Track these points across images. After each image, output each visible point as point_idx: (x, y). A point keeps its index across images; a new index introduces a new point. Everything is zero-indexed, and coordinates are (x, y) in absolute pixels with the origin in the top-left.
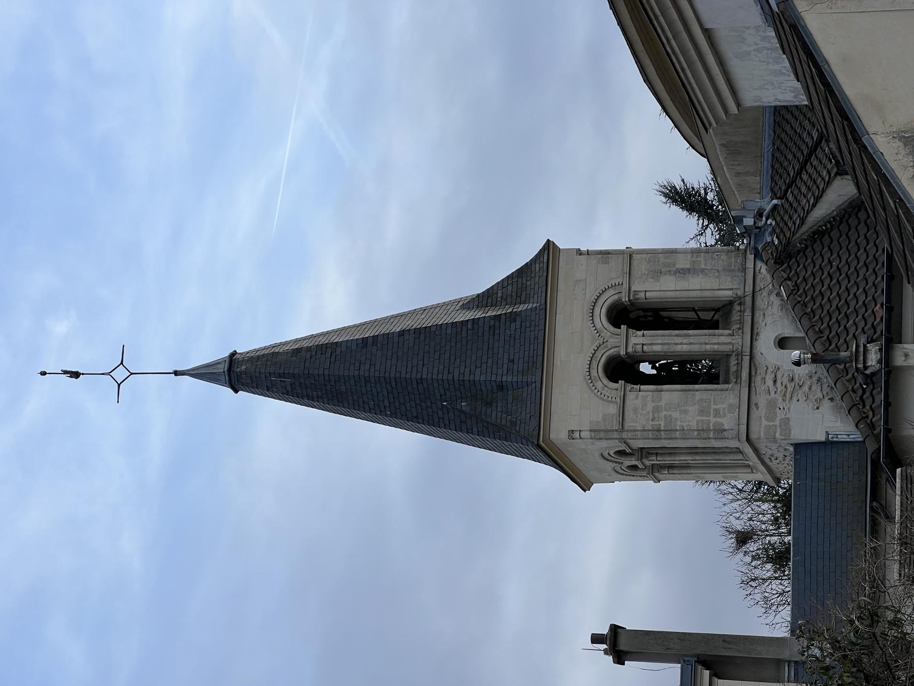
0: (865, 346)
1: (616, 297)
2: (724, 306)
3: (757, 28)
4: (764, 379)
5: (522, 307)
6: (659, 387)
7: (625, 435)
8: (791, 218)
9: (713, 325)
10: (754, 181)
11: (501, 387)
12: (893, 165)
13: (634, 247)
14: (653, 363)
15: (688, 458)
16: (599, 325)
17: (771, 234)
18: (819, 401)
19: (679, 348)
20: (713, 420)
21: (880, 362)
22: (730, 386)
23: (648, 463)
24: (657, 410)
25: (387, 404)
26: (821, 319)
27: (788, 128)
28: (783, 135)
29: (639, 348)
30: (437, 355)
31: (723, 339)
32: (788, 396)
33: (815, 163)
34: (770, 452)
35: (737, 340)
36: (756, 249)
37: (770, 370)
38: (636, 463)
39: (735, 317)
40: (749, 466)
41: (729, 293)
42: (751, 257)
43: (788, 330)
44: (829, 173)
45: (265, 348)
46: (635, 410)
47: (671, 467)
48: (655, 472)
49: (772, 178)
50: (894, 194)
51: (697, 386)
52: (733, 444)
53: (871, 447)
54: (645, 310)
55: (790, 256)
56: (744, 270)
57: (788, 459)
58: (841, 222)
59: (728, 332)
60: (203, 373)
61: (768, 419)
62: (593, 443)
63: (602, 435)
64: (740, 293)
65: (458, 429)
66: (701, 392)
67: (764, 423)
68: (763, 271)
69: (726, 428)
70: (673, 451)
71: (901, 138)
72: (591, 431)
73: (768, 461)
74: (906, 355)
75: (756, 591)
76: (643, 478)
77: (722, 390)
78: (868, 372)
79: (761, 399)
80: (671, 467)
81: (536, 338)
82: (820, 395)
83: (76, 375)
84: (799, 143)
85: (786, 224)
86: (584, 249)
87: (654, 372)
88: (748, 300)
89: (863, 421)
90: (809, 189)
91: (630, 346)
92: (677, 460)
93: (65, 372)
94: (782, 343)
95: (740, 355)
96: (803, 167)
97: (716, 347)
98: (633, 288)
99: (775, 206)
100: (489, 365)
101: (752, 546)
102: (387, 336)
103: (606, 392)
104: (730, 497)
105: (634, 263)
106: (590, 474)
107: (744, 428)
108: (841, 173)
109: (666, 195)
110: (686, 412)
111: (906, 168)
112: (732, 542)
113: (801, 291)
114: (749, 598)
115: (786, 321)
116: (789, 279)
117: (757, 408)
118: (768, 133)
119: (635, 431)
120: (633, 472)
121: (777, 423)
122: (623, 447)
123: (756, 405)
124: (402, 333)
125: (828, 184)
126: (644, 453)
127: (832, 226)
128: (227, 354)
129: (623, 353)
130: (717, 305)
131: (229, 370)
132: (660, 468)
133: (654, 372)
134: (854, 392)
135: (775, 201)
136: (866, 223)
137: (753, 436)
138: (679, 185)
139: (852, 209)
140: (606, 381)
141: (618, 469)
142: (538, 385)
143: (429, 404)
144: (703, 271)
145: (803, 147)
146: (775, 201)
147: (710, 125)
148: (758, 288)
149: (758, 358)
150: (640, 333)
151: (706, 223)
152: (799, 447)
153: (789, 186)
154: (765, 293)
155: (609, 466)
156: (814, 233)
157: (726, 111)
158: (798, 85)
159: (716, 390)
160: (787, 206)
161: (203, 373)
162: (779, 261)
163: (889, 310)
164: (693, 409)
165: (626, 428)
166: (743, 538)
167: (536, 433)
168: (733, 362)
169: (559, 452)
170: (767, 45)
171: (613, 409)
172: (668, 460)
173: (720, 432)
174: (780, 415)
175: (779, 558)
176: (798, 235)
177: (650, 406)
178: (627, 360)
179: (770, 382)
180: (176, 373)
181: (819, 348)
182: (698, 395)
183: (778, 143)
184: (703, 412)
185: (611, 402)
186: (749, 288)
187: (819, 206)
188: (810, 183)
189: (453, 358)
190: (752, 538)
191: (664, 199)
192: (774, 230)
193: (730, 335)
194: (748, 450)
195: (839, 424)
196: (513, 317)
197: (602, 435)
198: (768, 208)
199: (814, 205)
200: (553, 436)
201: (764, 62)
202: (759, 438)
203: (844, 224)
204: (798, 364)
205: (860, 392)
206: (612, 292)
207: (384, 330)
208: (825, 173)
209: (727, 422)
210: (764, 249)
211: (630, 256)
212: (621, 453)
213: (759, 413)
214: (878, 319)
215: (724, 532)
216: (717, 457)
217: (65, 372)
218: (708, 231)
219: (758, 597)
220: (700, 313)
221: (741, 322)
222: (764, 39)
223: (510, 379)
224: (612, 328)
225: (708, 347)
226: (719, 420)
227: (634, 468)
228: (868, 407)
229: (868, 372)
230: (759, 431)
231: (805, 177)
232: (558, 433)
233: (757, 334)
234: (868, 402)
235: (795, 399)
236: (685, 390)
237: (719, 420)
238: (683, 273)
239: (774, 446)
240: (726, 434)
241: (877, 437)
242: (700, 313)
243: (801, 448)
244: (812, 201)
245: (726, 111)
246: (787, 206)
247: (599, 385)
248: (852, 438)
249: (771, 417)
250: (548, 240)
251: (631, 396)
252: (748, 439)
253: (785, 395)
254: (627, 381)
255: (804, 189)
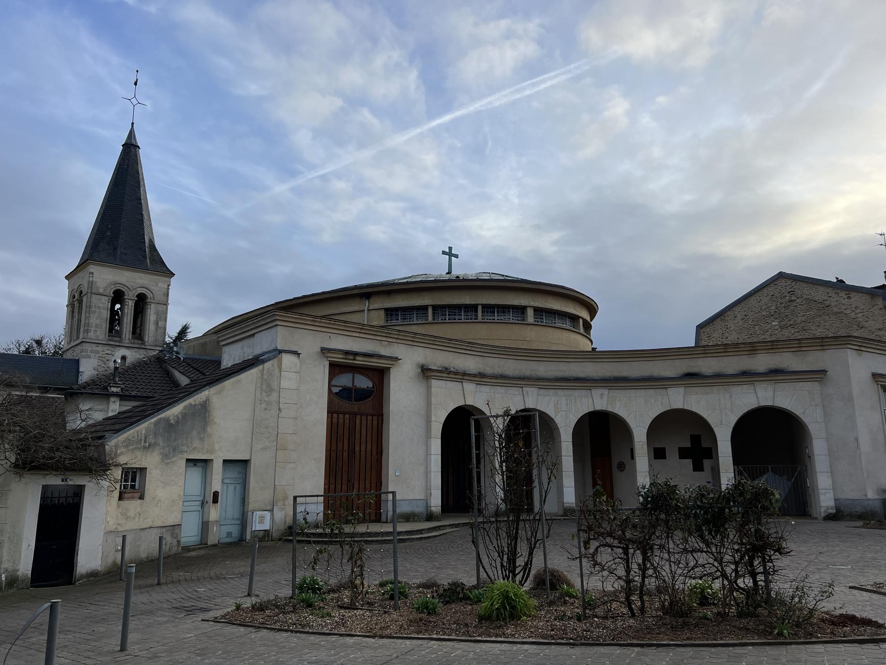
0: (120, 387)
1: (149, 297)
2: (142, 338)
3: (253, 353)
4: (109, 350)
5: (148, 261)
6: (109, 310)
7: (89, 294)
8: (175, 364)
9: (134, 333)
10: (191, 352)
11: (115, 249)
12: (196, 397)
13: (169, 306)
14: (120, 309)
15: (76, 319)
16: (138, 289)
17: (169, 356)
18: (97, 370)
19: (125, 319)
20: (93, 329)
21: (113, 392)
22: (107, 337)
23: (75, 303)
24: (99, 308)
25: (112, 204)
26: (133, 372)
27: (210, 365)
28: (208, 363)
29: (127, 304)
30: (131, 226)
31: (127, 336)
32: (100, 358)
33: (196, 373)
34: (76, 350)
35: (127, 341)
36: (164, 351)
37: (113, 353)
38: (76, 298)
39: (136, 341)
40: (71, 342)
41: (147, 340)
42: (161, 349)
43: (128, 361)
44: (192, 377)
45: (140, 161)
46: (99, 299)
47: (73, 312)
48: (71, 305)
49: (191, 358)
50: (185, 396)
51: (108, 324)
52: (81, 336)
53: (75, 387)
54: (143, 308)
55: (159, 362)
56: (156, 346)
57: (73, 357)
58: (171, 381)
59: (130, 338)
60: (131, 134)
61: (91, 350)
62: (86, 281)
63: (90, 285)
64: (146, 344)
65: (98, 230)
66: (105, 326)
67: (90, 349)
68: (155, 353)
69: (89, 334)
70: (80, 313)
71: (206, 400)
72: (92, 281)
73: (72, 349)
74: (114, 402)
75: (14, 346)
76: (69, 301)
77: (105, 334)
78: (108, 387)
79: (100, 348)
80: (73, 312)
81: (135, 265)
82: (100, 370)
83: (136, 84)
84: (204, 368)
85: (173, 362)
86: (170, 287)
87: (116, 309)
88: (143, 347)
89: (87, 384)
90: (186, 370)
91: (128, 300)
92: (76, 315)
93: (137, 80)
94: (124, 358)
95: (120, 342)
96: (195, 369)
97: (125, 333)
98: (152, 304)
99: (180, 359)
100: (125, 246)
101: (35, 345)
102: (141, 209)
103: (109, 289)
104: (58, 339)
105: (162, 306)
106: (72, 280)
107: (88, 341)
108: (192, 381)
109: (186, 325)
110: (97, 319)
111: (195, 401)
112: (37, 338)
113: (145, 366)
114: (11, 343)
115: (133, 360)
116: (151, 361)
117: (96, 347)
118: (209, 358)
119: (91, 299)
120: (72, 297)
121: (89, 354)
122: (84, 293)
123: (98, 346)
124: (142, 214)
125: (188, 377)
126: (80, 302)
127: (171, 378)
128: (139, 145)
129: (126, 297)
130: (142, 335)
131: (132, 144)
132: (73, 308)
133: (116, 309)
134: (100, 382)
135: (182, 359)
136: (171, 390)
137: (84, 344)
138: (188, 331)
139: (176, 384)
140: (114, 289)
141: (74, 291)
142: (115, 263)
143: (110, 220)
144: (157, 330)
145: (203, 369)
146: (182, 359)
147: (217, 335)
148: (147, 350)
149: (118, 348)
150: (133, 305)
151: (173, 339)
152: (78, 361)
153: (188, 364)
154: (145, 353)
155: (76, 287)
156: (168, 371)
157: (221, 341)
158: (229, 366)
159: (106, 331)
160: (180, 362)
161: (131, 134)
162: (158, 358)
163: (134, 397)
164: (98, 322)
165: (92, 295)
166: (39, 343)
167: (93, 259)
168: (117, 339)
169: (85, 267)
170: (246, 356)
171: (101, 291)
172: (76, 311)
173: (88, 331)
174: (92, 355)
175: (27, 351)
176: (168, 366)
177: (101, 305)
178: (122, 299)
179: (107, 352)
180: (133, 123)
181: (120, 370)
182: (104, 324)
183: (205, 361)
184: (97, 326)
185: (104, 290)
186: (148, 347)
187: (180, 373)
188: (189, 371)
189: (130, 232)
190: (38, 346)
191: (184, 325)
192: (171, 358)
193: (129, 338)
194: (78, 342)
195: (86, 377)
196: (145, 257)
197: (90, 285)
198: (180, 356)
199: (180, 372)
200: (91, 266)
201: (4, 631)
202: (83, 346)
203: (171, 382)
204: (115, 361)
205: (100, 384)
206: (151, 296)
207: (144, 208)
208: (192, 376)
209: (91, 335)
210: (163, 353)
211: (165, 304)
212: (81, 292)
213: (94, 347)
214: (131, 392)
215: (42, 335)
216: (76, 330)
217: (137, 80)
218: (170, 339)
219: (11, 346)
220: (139, 328)
221: (134, 343)
222: (248, 355)
223: (119, 252)
224: (136, 294)
225: (125, 330)
226: (92, 332)
227: (74, 297)
228: (93, 387)
229: (108, 387)
230: (86, 346)
231: (191, 369)
232: (92, 268)
233: (128, 349)
234: (95, 387)
235: (99, 361)
236: (107, 320)
237: (92, 332)
238: (157, 323)
239: (78, 352)
240: (86, 333)
241: (80, 390)
242: (139, 328)
243: (77, 362)
244: (181, 371)
245: (221, 341)
246: (180, 362)
247: (113, 287)
248: (80, 378)
249: (92, 351)
250: (175, 274)
251: (106, 298)
252: (82, 342)
253: (101, 357)
254: (113, 297)
255: (186, 368)
